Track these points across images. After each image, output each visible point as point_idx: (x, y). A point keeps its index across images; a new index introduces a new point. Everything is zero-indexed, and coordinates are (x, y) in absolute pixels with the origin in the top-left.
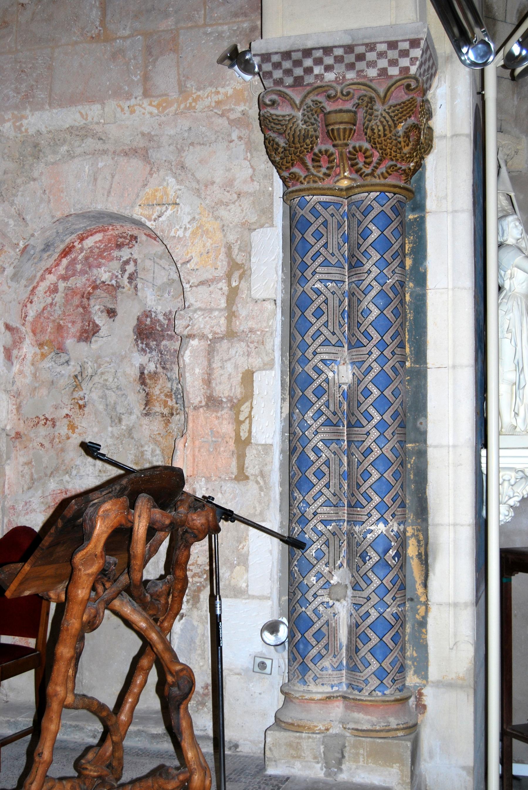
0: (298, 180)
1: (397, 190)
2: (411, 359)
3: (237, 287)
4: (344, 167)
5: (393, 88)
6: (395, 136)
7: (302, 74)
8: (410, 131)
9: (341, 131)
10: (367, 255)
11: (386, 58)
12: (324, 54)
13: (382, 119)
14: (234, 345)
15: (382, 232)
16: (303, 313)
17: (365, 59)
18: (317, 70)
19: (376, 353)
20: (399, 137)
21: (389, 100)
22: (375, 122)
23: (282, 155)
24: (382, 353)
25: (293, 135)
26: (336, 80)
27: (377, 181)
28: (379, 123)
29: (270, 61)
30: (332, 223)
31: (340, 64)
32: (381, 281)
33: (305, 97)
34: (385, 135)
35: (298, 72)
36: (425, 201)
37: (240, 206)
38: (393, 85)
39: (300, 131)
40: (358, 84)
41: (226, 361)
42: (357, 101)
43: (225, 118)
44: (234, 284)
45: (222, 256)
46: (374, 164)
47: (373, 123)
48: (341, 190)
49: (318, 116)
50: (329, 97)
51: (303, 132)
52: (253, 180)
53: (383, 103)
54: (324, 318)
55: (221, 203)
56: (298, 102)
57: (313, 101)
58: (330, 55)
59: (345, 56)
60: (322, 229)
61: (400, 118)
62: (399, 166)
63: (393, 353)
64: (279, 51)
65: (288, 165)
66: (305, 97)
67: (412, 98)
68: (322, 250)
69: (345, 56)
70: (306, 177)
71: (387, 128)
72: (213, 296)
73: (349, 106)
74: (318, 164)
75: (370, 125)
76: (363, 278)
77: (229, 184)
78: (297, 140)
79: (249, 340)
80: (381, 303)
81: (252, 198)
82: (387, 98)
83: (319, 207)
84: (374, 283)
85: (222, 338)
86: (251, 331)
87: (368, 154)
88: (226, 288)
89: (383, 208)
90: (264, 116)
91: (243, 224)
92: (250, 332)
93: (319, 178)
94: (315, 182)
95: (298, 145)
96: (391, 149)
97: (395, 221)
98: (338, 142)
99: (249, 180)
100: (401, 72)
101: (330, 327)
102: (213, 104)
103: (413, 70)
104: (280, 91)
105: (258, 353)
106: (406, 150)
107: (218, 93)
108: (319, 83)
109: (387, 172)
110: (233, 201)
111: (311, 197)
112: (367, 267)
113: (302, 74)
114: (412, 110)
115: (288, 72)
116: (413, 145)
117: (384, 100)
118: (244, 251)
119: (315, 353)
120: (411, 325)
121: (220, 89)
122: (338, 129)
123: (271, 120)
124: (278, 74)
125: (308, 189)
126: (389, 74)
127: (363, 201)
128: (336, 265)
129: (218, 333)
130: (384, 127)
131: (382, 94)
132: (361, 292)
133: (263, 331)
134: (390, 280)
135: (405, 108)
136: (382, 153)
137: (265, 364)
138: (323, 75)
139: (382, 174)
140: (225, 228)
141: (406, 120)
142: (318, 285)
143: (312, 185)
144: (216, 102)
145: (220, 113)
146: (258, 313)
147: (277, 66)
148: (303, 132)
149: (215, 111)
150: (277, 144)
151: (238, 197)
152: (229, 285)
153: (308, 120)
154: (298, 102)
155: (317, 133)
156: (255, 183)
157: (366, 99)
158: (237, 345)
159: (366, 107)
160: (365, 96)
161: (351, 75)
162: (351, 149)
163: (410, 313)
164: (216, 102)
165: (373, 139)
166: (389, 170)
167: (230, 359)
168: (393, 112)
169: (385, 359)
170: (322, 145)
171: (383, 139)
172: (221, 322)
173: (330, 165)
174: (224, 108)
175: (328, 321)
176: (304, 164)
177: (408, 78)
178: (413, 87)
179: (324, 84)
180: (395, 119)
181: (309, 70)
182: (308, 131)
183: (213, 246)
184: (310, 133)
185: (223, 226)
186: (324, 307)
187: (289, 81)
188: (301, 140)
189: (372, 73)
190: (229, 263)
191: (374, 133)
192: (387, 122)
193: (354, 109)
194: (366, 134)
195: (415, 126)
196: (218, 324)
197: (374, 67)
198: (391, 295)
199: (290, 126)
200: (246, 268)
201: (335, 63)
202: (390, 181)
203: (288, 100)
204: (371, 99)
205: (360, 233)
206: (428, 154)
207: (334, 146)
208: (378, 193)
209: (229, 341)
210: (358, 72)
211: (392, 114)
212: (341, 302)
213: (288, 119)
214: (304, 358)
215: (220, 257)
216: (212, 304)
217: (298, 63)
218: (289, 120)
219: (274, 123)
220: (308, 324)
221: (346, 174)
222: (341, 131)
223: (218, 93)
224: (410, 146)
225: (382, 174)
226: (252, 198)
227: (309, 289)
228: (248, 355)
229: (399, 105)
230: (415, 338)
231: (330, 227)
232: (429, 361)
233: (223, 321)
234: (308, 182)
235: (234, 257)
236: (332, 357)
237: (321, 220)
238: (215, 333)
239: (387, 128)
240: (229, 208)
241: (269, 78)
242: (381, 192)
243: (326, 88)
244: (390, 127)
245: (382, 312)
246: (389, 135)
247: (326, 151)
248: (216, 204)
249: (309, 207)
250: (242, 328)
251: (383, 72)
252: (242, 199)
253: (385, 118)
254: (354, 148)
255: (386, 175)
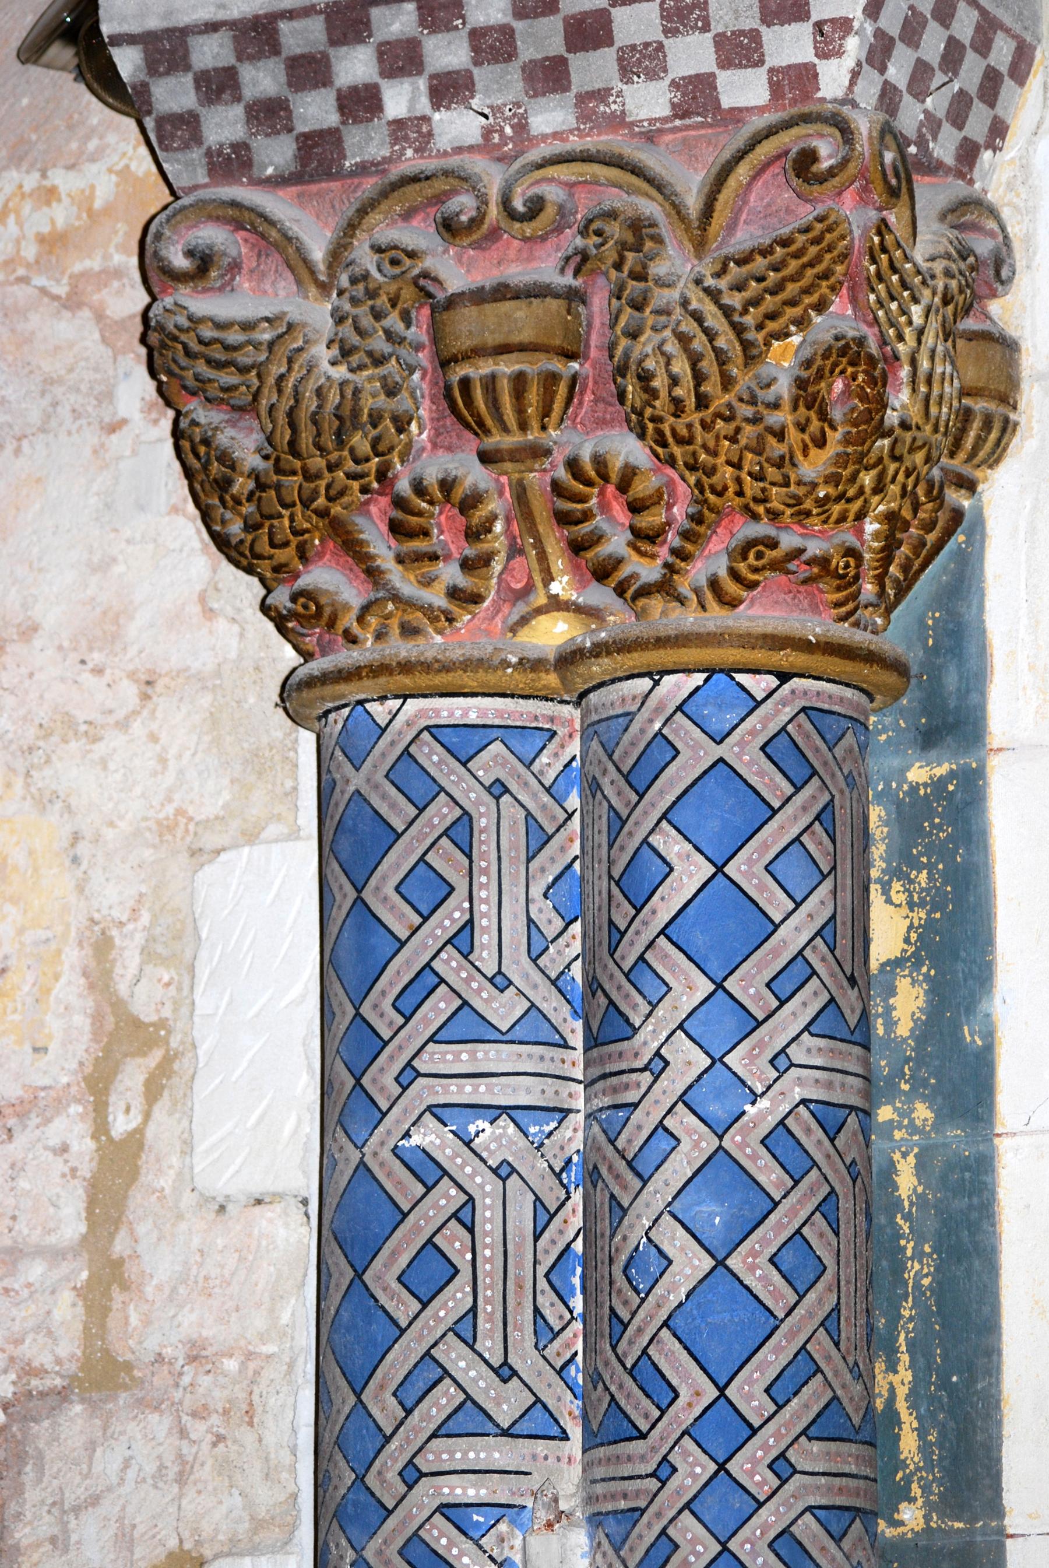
0: (331, 624)
1: (786, 659)
2: (926, 1489)
3: (136, 1140)
4: (542, 556)
5: (742, 172)
6: (753, 401)
7: (333, 119)
8: (820, 376)
9: (505, 389)
10: (647, 981)
11: (706, 28)
12: (422, 22)
13: (689, 326)
14: (116, 1427)
15: (720, 869)
16: (359, 1275)
17: (608, 40)
18: (400, 99)
19: (693, 1468)
20: (776, 406)
21: (732, 227)
22: (657, 338)
23: (248, 509)
24: (722, 1467)
25: (291, 414)
26: (487, 145)
27: (688, 619)
28: (672, 347)
29: (188, 68)
30: (499, 829)
31: (498, 68)
32: (715, 1110)
33: (351, 228)
34: (702, 402)
35: (316, 110)
36: (983, 694)
37: (153, 738)
38: (740, 156)
39: (319, 392)
40: (586, 158)
41: (77, 1510)
42: (579, 241)
43: (86, 313)
44: (121, 1125)
45: (70, 988)
46: (673, 538)
47: (647, 342)
48: (532, 665)
49: (406, 318)
50: (449, 228)
51: (333, 398)
52: (209, 613)
53: (700, 246)
54: (456, 1298)
55: (66, 726)
56: (318, 254)
57: (378, 249)
58: (450, 28)
59: (519, 25)
60: (447, 862)
61: (772, 316)
62: (789, 540)
63: (782, 1467)
64: (222, 15)
65: (282, 555)
66: (351, 228)
67: (820, 219)
68: (449, 964)
69: (519, 25)
70: (366, 609)
71: (708, 365)
72: (23, 1184)
73: (546, 268)
74: (418, 545)
75: (635, 355)
76: (632, 1096)
77: (103, 631)
78: (306, 439)
79: (187, 1403)
80: (714, 1215)
81: (205, 700)
82: (719, 219)
83: (431, 756)
84: (683, 1121)
85: (63, 1395)
86: (197, 1354)
87: (641, 488)
88: (83, 1146)
89: (719, 751)
90: (161, 328)
91: (166, 828)
92: (192, 1359)
93: (431, 613)
94: (409, 631)
95: (318, 462)
96: (738, 466)
97: (789, 809)
98: (497, 440)
99: (195, 609)
100: (776, 90)
101: (489, 1345)
102: (30, 251)
103: (832, 79)
104: (234, 204)
105: (226, 1468)
106: (813, 466)
107: (50, 195)
108: (411, 162)
109: (734, 574)
110: (120, 714)
111: (396, 703)
112: (648, 1039)
113: (333, 119)
114: (826, 275)
115: (269, 114)
116: (847, 441)
117: (699, 231)
118: (164, 961)
119: (412, 1475)
120: (923, 1317)
121: (59, 178)
122: (491, 383)
123: (194, 346)
124: (224, 125)
125: (378, 670)
126: (726, 103)
127: (630, 716)
128: (518, 1033)
129: (40, 1372)
130: (695, 360)
131: (693, 203)
132: (621, 1166)
133: (249, 1356)
134: (763, 1103)
135: (794, 265)
136: (699, 484)
137: (259, 1525)
138: (426, 119)
139: (714, 584)
140: (83, 849)
141: (802, 323)
142: (428, 1137)
143: (399, 648)
144: (41, 239)
145: (61, 290)
146: (232, 1261)
147: (218, 85)
148: (333, 398)
149: (39, 281)
150: (225, 458)
151: (145, 697)
152: (101, 1128)
153: (355, 339)
154: (318, 254)
155: (403, 402)
156: (221, 624)
157: (615, 230)
158: (132, 1428)
159: (618, 266)
160: (612, 215)
161: (551, 117)
162: (562, 473)
163: (918, 1255)
164: (41, 239)
165: (654, 419)
166: (742, 567)
167: (95, 1500)
168: (739, 287)
169: (739, 1503)
170: (431, 455)
171: (695, 418)
172: (57, 1315)
173: (470, 552)
174: (78, 267)
175: (474, 1310)
176: (353, 550)
177: (806, 118)
178: (825, 165)
179: (429, 165)
180: (749, 320)
181: (361, 103)
182: (357, 392)
183: (28, 937)
184: (367, 404)
185: (76, 838)
186: (454, 1243)
187: (276, 154)
188: (329, 440)
189: (648, 101)
190: (97, 1018)
191: (654, 394)
192: (711, 335)
193: (568, 279)
194: (621, 396)
195: (843, 351)
196: (45, 1329)
197: (652, 75)
198: (770, 1176)
199: (277, 369)
200: (174, 1043)
201: (477, 63)
202: (765, 613)
203: (276, 245)
204: (640, 230)
205: (616, 875)
206: (994, 459)
207: (486, 458)
208: (699, 678)
209: (93, 1407)
210: (582, 99)
211: (735, 300)
212: (545, 1215)
213: (267, 337)
214: (363, 1497)
215: (59, 990)
216: (22, 1227)
217: (310, 71)
218: (271, 345)
219: (209, 362)
220: (381, 1330)
221: (555, 588)
222: (505, 389)
223: (50, 195)
224: (833, 447)
225: (714, 584)
226: (205, 700)
227: (386, 1154)
228: (181, 1479)
229: (766, 252)
230: (944, 1384)
231: (484, 846)
232: (1010, 1498)
233: (66, 1311)
234: (380, 636)
235: (123, 988)
236: (500, 1490)
237: (441, 814)
238: (30, 1371)
239: (708, 365)
240: (100, 749)
241: (186, 146)
242: (711, 671)
243: (440, 185)
244: (721, 358)
245: (721, 1263)
246: (720, 401)
247: (447, 485)
248: (45, 731)
249: (386, 751)
250: (152, 1343)
251: (697, 96)
252: (162, 703)
253: (698, 317)
254: (573, 465)
255: (732, 588)
